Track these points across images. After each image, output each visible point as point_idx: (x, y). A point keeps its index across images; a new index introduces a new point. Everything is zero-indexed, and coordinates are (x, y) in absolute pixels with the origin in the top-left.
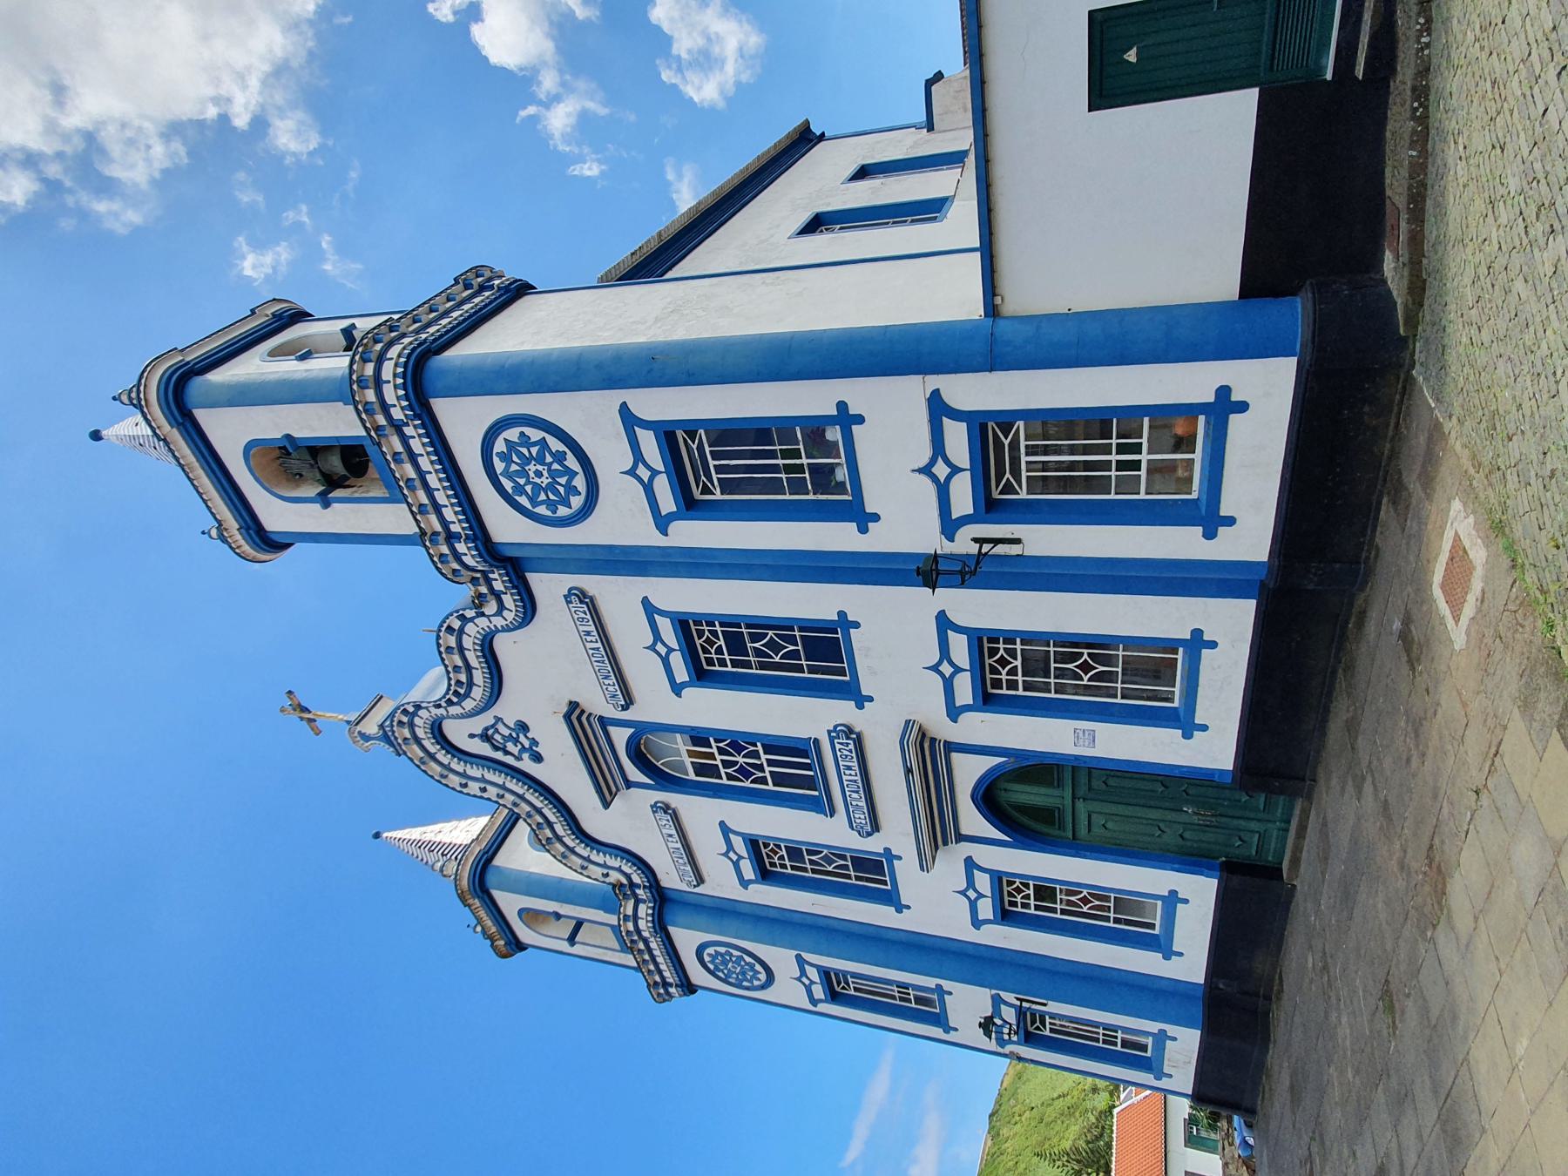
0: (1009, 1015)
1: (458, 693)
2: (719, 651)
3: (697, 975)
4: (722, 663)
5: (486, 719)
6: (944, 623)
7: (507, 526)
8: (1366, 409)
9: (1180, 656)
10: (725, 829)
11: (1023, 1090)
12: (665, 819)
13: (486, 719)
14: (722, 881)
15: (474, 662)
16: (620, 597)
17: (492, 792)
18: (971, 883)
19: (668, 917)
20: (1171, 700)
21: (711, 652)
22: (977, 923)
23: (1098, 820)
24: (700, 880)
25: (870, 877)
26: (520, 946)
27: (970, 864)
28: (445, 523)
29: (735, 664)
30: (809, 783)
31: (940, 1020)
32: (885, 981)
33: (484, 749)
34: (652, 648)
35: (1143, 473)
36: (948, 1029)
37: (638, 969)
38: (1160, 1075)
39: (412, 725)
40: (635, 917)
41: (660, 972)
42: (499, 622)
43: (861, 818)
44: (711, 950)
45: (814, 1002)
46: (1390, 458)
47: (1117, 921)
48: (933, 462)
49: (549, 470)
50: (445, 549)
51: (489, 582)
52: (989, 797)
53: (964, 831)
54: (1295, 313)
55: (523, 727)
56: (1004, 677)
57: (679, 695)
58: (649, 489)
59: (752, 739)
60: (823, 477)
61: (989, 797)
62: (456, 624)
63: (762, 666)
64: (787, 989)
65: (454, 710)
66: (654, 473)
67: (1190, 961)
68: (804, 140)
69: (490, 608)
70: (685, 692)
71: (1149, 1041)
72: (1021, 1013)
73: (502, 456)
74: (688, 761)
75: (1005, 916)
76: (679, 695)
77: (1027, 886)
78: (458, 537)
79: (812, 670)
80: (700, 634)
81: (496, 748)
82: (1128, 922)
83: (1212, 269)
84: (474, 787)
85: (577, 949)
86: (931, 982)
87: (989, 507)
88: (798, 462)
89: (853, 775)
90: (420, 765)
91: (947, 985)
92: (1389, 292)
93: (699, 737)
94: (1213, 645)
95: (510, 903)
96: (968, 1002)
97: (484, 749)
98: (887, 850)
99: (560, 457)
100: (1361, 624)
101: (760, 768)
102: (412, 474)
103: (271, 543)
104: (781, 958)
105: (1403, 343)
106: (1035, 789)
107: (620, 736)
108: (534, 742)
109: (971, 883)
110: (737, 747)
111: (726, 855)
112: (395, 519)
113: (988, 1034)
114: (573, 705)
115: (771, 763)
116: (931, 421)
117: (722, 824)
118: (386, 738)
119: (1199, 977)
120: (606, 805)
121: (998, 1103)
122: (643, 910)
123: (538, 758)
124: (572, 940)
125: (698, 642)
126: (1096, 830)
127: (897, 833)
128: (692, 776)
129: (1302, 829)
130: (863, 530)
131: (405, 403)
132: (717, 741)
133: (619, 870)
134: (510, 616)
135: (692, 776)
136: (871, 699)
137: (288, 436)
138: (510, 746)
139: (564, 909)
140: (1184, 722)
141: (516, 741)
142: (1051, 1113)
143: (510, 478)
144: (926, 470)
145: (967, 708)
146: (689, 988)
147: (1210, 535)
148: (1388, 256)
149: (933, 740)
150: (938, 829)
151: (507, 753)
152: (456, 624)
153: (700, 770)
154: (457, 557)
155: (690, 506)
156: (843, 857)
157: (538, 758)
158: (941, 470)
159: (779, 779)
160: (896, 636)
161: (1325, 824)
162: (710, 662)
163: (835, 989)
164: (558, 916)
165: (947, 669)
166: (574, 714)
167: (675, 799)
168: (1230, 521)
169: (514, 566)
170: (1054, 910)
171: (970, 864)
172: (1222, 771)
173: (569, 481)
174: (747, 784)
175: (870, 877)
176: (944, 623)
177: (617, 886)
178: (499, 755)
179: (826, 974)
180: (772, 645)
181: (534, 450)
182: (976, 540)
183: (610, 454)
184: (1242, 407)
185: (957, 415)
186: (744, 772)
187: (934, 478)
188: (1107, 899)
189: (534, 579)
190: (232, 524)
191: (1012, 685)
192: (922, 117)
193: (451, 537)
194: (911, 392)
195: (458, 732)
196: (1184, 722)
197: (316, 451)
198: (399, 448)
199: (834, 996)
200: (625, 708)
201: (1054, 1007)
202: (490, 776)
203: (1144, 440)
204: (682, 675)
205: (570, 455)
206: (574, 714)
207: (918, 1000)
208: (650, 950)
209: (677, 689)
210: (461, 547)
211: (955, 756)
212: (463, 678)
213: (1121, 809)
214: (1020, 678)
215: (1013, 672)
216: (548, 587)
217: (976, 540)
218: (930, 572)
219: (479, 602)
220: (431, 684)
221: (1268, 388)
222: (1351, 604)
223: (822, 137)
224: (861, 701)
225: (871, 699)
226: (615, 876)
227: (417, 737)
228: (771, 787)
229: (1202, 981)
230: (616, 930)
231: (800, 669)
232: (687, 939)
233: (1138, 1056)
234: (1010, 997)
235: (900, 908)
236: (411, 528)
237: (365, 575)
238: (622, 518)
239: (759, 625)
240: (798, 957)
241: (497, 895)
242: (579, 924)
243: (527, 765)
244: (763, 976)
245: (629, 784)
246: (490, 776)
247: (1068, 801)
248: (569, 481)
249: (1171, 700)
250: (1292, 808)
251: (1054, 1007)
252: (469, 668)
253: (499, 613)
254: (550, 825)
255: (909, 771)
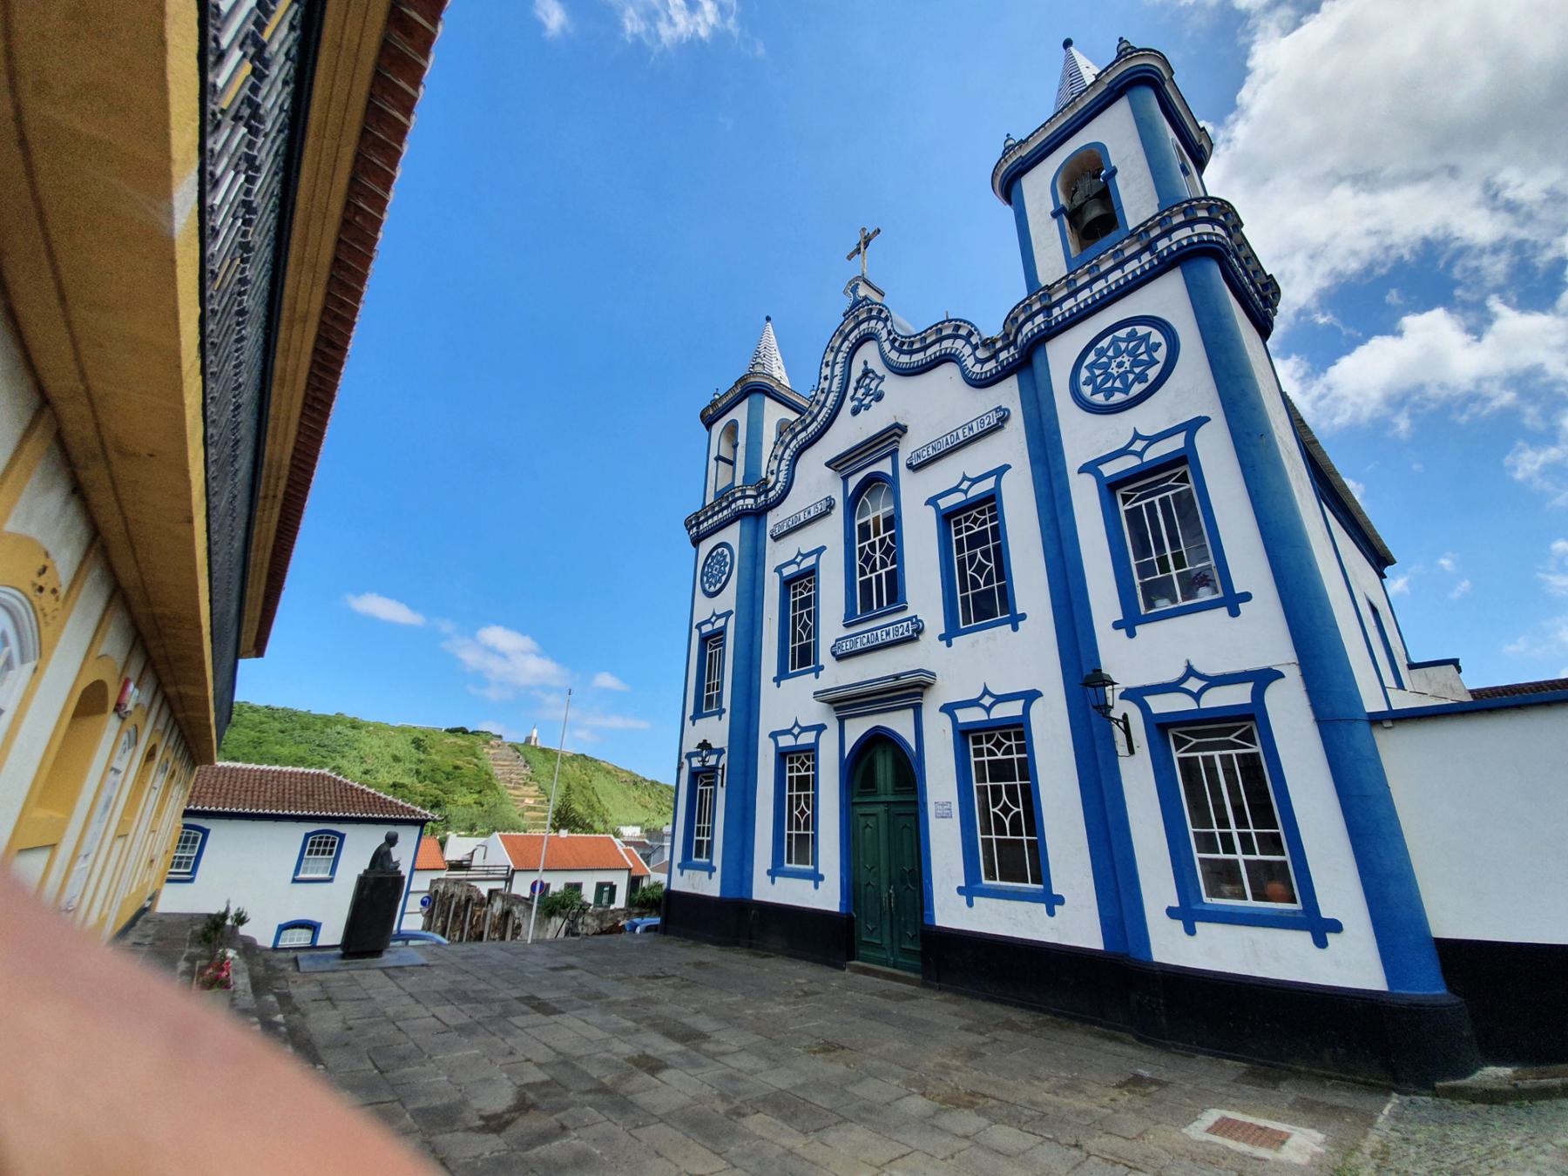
0: (712, 761)
1: (903, 345)
2: (968, 528)
3: (707, 546)
4: (958, 532)
5: (880, 369)
6: (1030, 696)
7: (1061, 355)
8: (1341, 1051)
9: (1030, 885)
10: (819, 551)
11: (600, 775)
12: (822, 507)
13: (880, 369)
14: (778, 554)
15: (930, 351)
16: (1011, 446)
17: (825, 385)
18: (805, 729)
19: (746, 520)
20: (790, 861)
21: (972, 526)
22: (774, 735)
23: (871, 821)
24: (776, 539)
25: (800, 657)
26: (709, 426)
27: (820, 728)
28: (1059, 303)
29: (960, 542)
30: (867, 605)
31: (698, 714)
32: (720, 674)
33: (856, 372)
34: (965, 478)
35: (1222, 856)
36: (694, 719)
37: (704, 506)
38: (682, 867)
39: (869, 319)
40: (744, 497)
41: (707, 519)
42: (970, 362)
43: (847, 647)
44: (726, 552)
45: (699, 626)
46: (1289, 1070)
47: (790, 836)
48: (992, 695)
49: (1126, 372)
50: (1036, 307)
51: (1006, 347)
52: (878, 740)
53: (847, 723)
54: (1430, 987)
55: (879, 397)
56: (985, 746)
57: (927, 503)
58: (1123, 452)
59: (898, 559)
60: (1155, 591)
61: (878, 740)
62: (963, 332)
63: (961, 563)
64: (705, 608)
65: (887, 346)
66: (1140, 454)
67: (767, 889)
68: (1380, 559)
69: (981, 354)
70: (931, 509)
71: (704, 860)
72: (714, 769)
73: (1134, 333)
74: (870, 518)
75: (783, 755)
76: (927, 503)
77: (807, 770)
78: (1049, 314)
79: (965, 600)
80: (982, 513)
81: (858, 382)
82: (790, 844)
83: (1457, 912)
84: (826, 371)
85: (712, 463)
86: (726, 703)
87: (1160, 727)
88: (1172, 567)
89: (882, 637)
90: (839, 331)
91: (726, 716)
92: (1473, 1072)
93: (892, 522)
94: (816, 887)
95: (740, 414)
96: (717, 730)
97: (856, 372)
98: (822, 668)
99: (1141, 378)
100: (1112, 1039)
101: (873, 570)
102: (1103, 268)
103: (1009, 185)
104: (728, 599)
105: (1424, 1083)
106: (889, 775)
107: (885, 466)
108: (868, 407)
109: (805, 729)
110: (888, 551)
111: (799, 553)
112: (1052, 264)
113: (700, 746)
114: (904, 429)
115: (879, 577)
116: (1246, 672)
117: (824, 548)
118: (856, 304)
119: (757, 895)
120: (828, 464)
121: (592, 760)
122: (750, 501)
123: (855, 412)
124: (719, 458)
125: (974, 512)
126: (862, 820)
127: (837, 675)
128: (858, 522)
129: (895, 978)
130: (1117, 625)
131: (1174, 248)
132: (891, 537)
133: (777, 481)
134: (977, 368)
135: (858, 522)
136: (949, 645)
137: (1114, 171)
138: (862, 391)
139: (741, 451)
140: (775, 872)
141: (866, 394)
142: (589, 793)
143: (1112, 344)
144: (986, 692)
145: (954, 719)
146: (696, 542)
147: (1172, 913)
148: (1506, 1071)
149: (921, 695)
150: (845, 704)
151: (856, 390)
152: (963, 332)
153: (864, 529)
154: (1030, 318)
155: (1110, 488)
156: (809, 637)
157: (855, 412)
158: (987, 701)
159: (866, 585)
160: (1014, 661)
161: (913, 997)
162: (958, 523)
163: (711, 640)
164: (735, 446)
165: (987, 701)
166: (897, 431)
167: (838, 512)
168: (970, 904)
169: (1024, 361)
170: (791, 790)
171: (820, 728)
172: (932, 916)
173: (1118, 390)
174: (858, 562)
175: (800, 657)
176: (1030, 696)
177: (766, 481)
178: (853, 384)
179: (721, 632)
180: (981, 568)
181: (1097, 372)
182: (1125, 716)
183: (1152, 417)
184: (1051, 913)
185: (1026, 709)
186: (867, 559)
187: (1184, 679)
188: (806, 828)
189: (1012, 383)
190: (1024, 152)
191: (979, 753)
192: (1415, 661)
193: (1047, 309)
194: (1276, 649)
195: (869, 353)
196: (775, 872)
197: (1106, 195)
198: (1127, 253)
199: (704, 640)
200: (910, 466)
201: (721, 794)
202: (836, 381)
203: (1258, 857)
204: (945, 503)
205: (1143, 386)
206: (897, 431)
207: (710, 698)
208: (722, 510)
209: (932, 502)
210: (1040, 319)
211: (910, 712)
212: (916, 346)
213: (883, 838)
214: (986, 758)
215: (991, 753)
216: (1008, 394)
217: (1125, 716)
218: (1085, 681)
219: (988, 343)
220: (907, 324)
221: (1352, 963)
222: (1121, 1030)
223: (1382, 576)
224: (947, 638)
225: (949, 645)
226: (772, 479)
227: (863, 318)
228: (859, 579)
229: (755, 897)
230: (731, 486)
231: (964, 589)
232: (732, 535)
233: (695, 851)
234: (724, 760)
235: (777, 680)
236: (1045, 279)
237: (983, 265)
238: (1085, 437)
239: (1001, 556)
240: (730, 613)
241: (745, 403)
242: (732, 463)
243: (848, 405)
244: (712, 589)
245: (845, 479)
246: (836, 381)
247: (883, 798)
248: (1118, 390)
249: (790, 861)
250: (915, 972)
251: (721, 794)
252: (924, 349)
253: (978, 361)
254: (804, 429)
255: (897, 677)
